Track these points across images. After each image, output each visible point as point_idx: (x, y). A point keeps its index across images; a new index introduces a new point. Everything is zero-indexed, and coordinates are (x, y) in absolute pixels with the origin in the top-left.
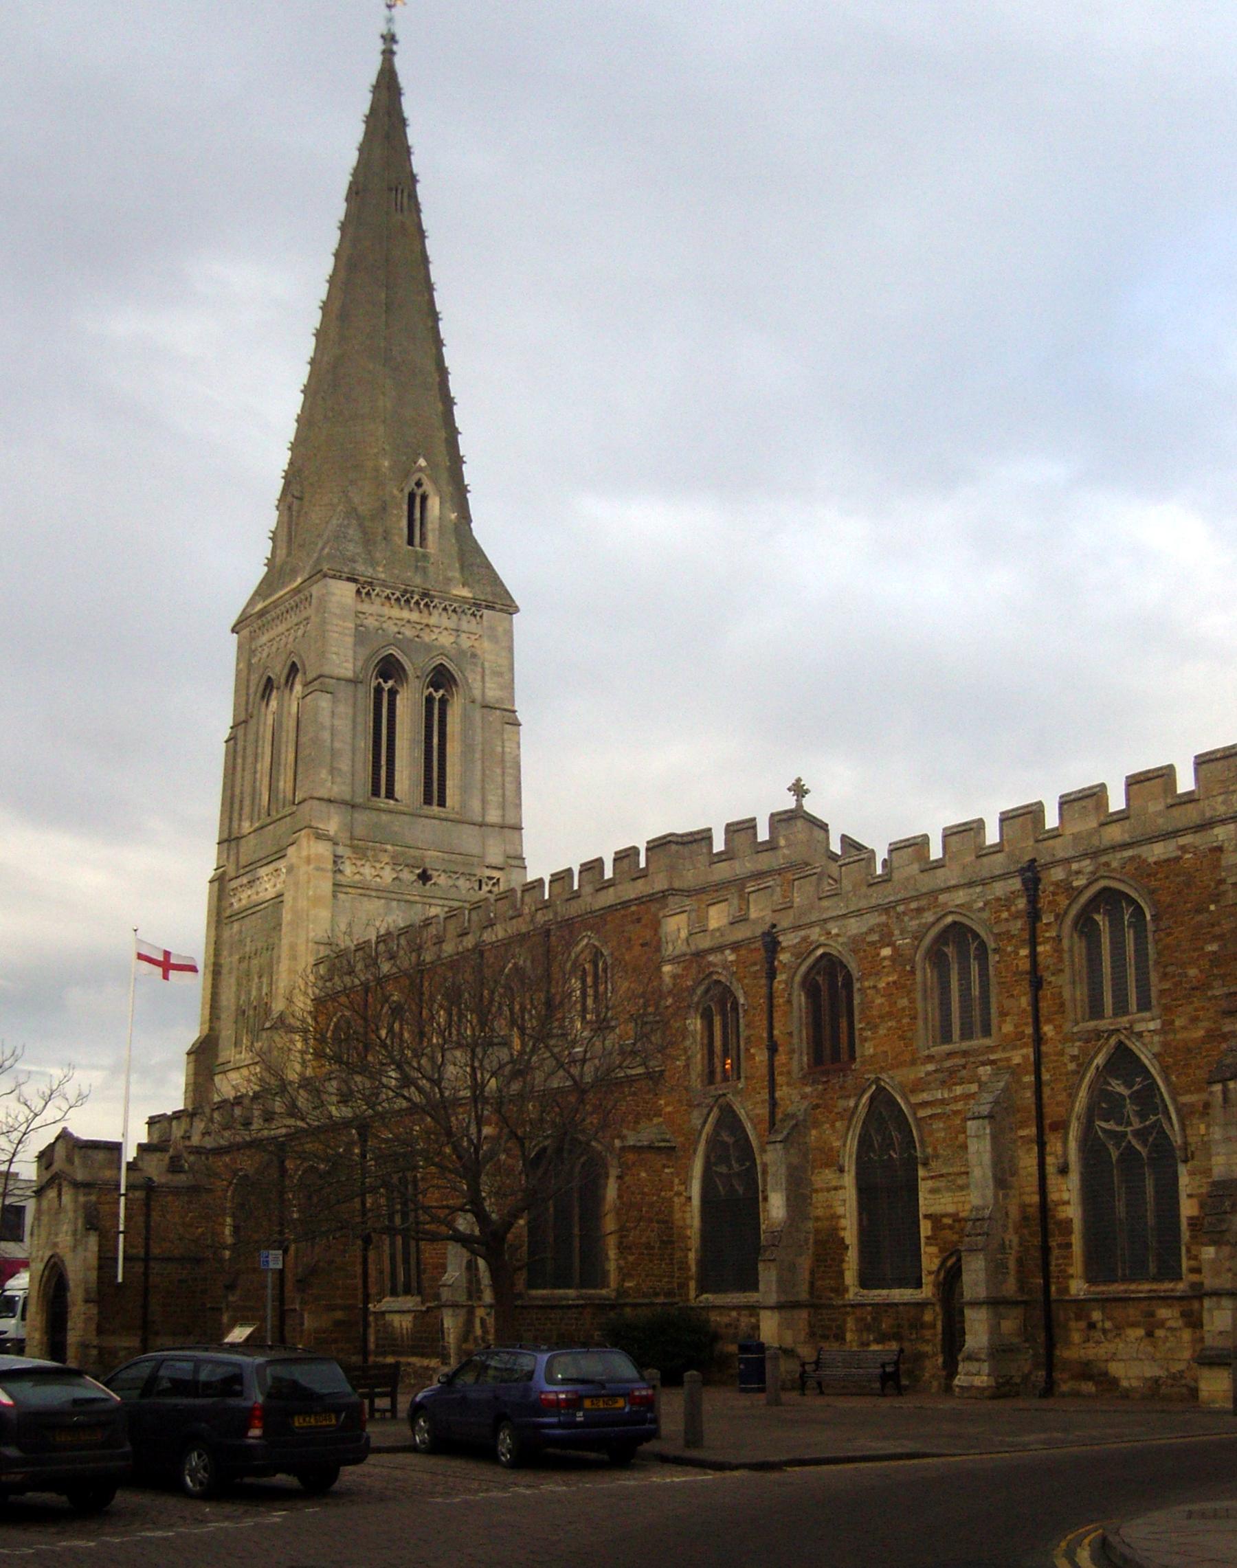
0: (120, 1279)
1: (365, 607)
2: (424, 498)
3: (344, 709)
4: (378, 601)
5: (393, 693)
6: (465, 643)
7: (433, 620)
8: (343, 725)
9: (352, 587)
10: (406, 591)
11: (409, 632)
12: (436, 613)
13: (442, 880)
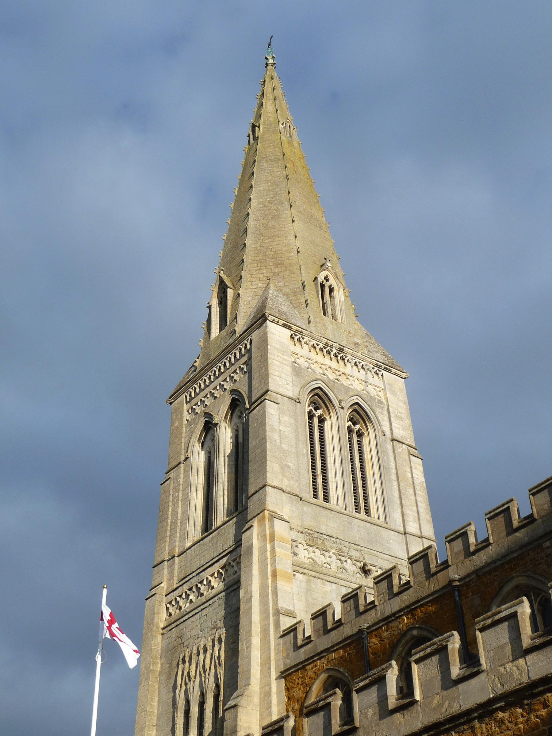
0: (105, 591)
1: (297, 349)
2: (331, 290)
4: (306, 347)
9: (288, 332)
10: (327, 344)
11: (332, 377)
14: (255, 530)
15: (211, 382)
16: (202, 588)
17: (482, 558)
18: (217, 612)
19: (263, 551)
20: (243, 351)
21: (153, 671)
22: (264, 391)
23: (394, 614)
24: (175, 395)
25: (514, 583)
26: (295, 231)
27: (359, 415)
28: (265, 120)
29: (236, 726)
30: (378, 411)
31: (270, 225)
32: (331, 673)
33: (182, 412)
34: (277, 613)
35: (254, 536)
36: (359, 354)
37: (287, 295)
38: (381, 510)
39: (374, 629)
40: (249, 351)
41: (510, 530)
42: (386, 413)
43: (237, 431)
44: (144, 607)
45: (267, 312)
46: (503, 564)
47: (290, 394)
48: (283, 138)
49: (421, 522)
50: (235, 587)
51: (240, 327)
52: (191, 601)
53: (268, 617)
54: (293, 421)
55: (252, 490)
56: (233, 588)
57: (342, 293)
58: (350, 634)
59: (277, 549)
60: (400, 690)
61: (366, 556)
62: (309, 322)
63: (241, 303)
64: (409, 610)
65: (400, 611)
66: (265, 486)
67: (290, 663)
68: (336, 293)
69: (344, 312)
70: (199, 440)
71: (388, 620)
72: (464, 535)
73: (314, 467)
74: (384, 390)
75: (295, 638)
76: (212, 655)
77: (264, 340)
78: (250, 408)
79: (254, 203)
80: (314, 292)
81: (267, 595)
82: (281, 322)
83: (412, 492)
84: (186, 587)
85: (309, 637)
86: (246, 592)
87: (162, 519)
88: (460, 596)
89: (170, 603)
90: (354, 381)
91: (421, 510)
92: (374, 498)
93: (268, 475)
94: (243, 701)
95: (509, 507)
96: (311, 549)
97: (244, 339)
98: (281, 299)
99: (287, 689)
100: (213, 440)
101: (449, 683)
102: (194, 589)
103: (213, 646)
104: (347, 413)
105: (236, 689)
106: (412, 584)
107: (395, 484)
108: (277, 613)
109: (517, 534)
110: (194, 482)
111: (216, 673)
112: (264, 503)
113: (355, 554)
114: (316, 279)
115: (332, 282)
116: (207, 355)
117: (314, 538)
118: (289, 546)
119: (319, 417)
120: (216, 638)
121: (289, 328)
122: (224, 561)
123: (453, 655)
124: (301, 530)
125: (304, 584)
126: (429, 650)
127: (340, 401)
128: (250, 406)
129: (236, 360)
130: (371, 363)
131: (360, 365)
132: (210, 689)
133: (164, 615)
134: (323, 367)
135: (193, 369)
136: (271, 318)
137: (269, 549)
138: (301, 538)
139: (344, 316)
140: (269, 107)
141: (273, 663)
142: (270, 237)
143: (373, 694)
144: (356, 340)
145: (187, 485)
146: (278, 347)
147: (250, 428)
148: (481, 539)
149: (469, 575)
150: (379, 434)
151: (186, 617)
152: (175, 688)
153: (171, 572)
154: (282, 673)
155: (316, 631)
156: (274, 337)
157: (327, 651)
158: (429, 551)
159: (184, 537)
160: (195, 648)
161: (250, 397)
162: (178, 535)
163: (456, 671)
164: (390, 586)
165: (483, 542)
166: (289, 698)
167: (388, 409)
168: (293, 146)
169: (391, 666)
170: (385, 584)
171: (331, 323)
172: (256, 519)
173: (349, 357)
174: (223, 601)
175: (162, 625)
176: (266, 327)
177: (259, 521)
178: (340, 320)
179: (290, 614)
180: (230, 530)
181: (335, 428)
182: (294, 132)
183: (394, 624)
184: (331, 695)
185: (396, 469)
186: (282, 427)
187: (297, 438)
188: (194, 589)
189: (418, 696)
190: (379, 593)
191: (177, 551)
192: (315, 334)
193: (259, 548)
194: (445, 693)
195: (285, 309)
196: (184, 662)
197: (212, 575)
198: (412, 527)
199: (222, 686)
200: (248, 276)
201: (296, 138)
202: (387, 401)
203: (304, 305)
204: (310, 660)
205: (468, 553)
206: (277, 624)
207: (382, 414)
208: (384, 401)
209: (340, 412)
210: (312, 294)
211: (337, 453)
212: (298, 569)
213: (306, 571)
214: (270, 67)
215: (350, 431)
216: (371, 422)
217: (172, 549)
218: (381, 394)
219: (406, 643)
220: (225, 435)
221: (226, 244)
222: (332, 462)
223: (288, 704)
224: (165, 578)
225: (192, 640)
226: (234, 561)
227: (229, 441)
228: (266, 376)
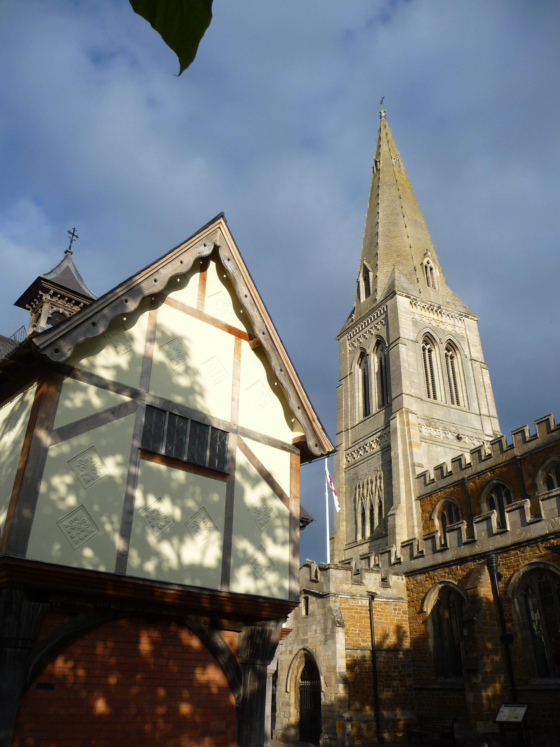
1: (414, 309)
2: (431, 269)
9: (408, 300)
10: (431, 305)
11: (435, 324)
13: (467, 440)
14: (398, 419)
15: (363, 329)
16: (367, 448)
17: (533, 445)
18: (377, 462)
19: (403, 431)
20: (382, 312)
21: (342, 492)
22: (397, 337)
23: (483, 471)
24: (341, 335)
25: (551, 459)
26: (408, 234)
27: (451, 346)
28: (383, 157)
29: (395, 525)
30: (462, 342)
31: (392, 229)
32: (447, 499)
33: (346, 346)
34: (414, 465)
35: (397, 422)
36: (450, 309)
37: (405, 275)
38: (466, 402)
39: (471, 478)
40: (386, 312)
41: (549, 431)
42: (466, 343)
43: (381, 358)
45: (396, 289)
46: (545, 449)
47: (412, 338)
48: (395, 168)
49: (490, 407)
50: (387, 449)
51: (379, 296)
52: (361, 455)
53: (408, 467)
54: (414, 354)
55: (394, 396)
56: (386, 450)
57: (438, 271)
58: (457, 480)
59: (411, 430)
60: (498, 524)
61: (459, 429)
62: (420, 292)
63: (379, 281)
64: (491, 469)
65: (486, 470)
66: (402, 394)
67: (422, 492)
68: (434, 271)
69: (440, 283)
70: (358, 362)
71: (479, 474)
72: (523, 432)
73: (427, 380)
74: (465, 329)
75: (425, 479)
76: (376, 485)
77: (395, 307)
78: (389, 346)
79: (381, 215)
80: (421, 272)
81: (407, 455)
82: (405, 294)
83: (484, 390)
84: (357, 447)
85: (433, 479)
86: (395, 453)
87: (339, 408)
88: (521, 464)
89: (348, 455)
90: (449, 325)
91: (489, 400)
92: (462, 395)
93: (403, 388)
94: (398, 512)
95: (548, 419)
96: (428, 428)
97: (382, 305)
98: (403, 279)
99: (422, 506)
100: (366, 362)
101: (524, 524)
102: (362, 448)
103: (376, 480)
104: (444, 345)
105: (392, 505)
106: (493, 456)
107: (473, 386)
108: (414, 465)
109: (553, 434)
110: (356, 387)
111: (379, 495)
112: (402, 404)
113: (453, 429)
114: (422, 264)
115: (432, 264)
117: (430, 422)
118: (417, 428)
119: (429, 349)
120: (378, 476)
122: (379, 434)
123: (527, 511)
124: (423, 417)
125: (426, 448)
126: (514, 507)
127: (440, 339)
128: (389, 346)
129: (378, 317)
130: (457, 313)
131: (450, 316)
132: (376, 503)
133: (345, 461)
134: (430, 319)
135: (350, 319)
136: (398, 293)
137: (406, 430)
138: (423, 422)
139: (440, 285)
140: (384, 148)
141: (412, 492)
142: (392, 238)
143: (484, 525)
144: (448, 300)
145: (353, 389)
146: (404, 310)
147: (390, 359)
148: (532, 434)
149: (526, 453)
150: (463, 357)
151: (358, 464)
152: (355, 501)
153: (347, 437)
154: (418, 497)
155: (436, 476)
156: (401, 304)
157: (444, 487)
158: (502, 439)
159: (353, 419)
160: (365, 481)
161: (388, 340)
162: (349, 417)
163: (529, 518)
164: (480, 456)
165: (533, 436)
166: (423, 511)
167: (468, 341)
168: (401, 173)
169: (493, 512)
170: (476, 454)
171: (433, 291)
172: (398, 413)
173: (444, 311)
174: (380, 456)
175: (344, 467)
176: (396, 298)
177: (400, 414)
178: (437, 289)
179: (421, 466)
180: (381, 418)
181: (438, 355)
182: (401, 164)
183: (482, 476)
184: (461, 523)
185: (474, 377)
186: (408, 358)
187: (418, 365)
188: (362, 448)
189: (509, 529)
190: (473, 459)
191: (350, 427)
192: (424, 300)
193: (401, 429)
194: (523, 528)
195: (405, 285)
196: (359, 488)
197: (373, 441)
198: (484, 411)
199: (383, 502)
200: (382, 264)
201: (403, 168)
202: (467, 336)
203: (416, 282)
205: (525, 442)
206: (414, 471)
207: (465, 344)
208: (465, 336)
209: (441, 345)
210: (420, 273)
211: (440, 370)
212: (422, 440)
214: (383, 118)
215: (446, 356)
216: (458, 350)
217: (346, 425)
218: (463, 332)
219: (490, 487)
220: (374, 361)
221: (365, 241)
222: (437, 376)
223: (422, 514)
224: (344, 441)
225: (363, 476)
226: (385, 434)
227: (376, 364)
228: (397, 329)
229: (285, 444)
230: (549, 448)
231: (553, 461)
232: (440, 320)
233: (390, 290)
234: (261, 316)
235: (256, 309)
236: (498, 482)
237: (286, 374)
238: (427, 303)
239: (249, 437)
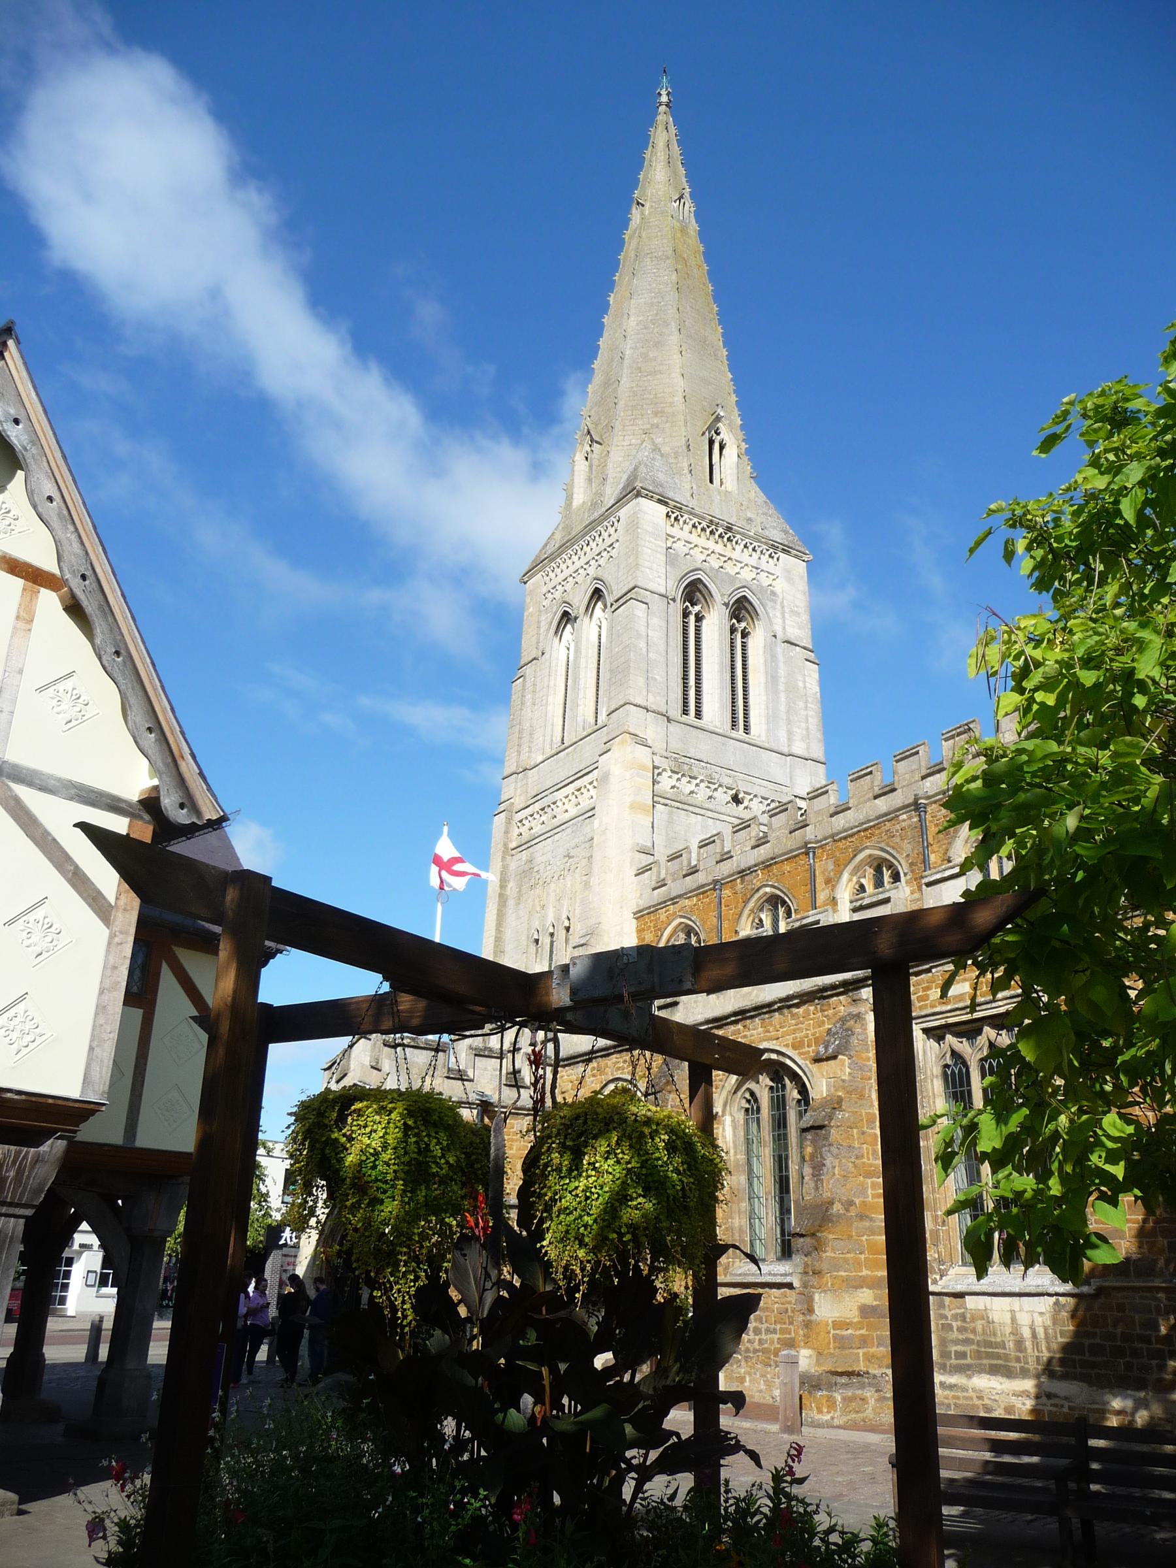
1: (675, 531)
2: (722, 447)
3: (655, 621)
5: (699, 618)
6: (764, 580)
7: (735, 555)
8: (657, 636)
9: (664, 510)
12: (739, 548)
25: (867, 852)
30: (770, 604)
31: (651, 355)
44: (492, 822)
61: (740, 783)
67: (643, 903)
73: (685, 677)
113: (726, 781)
116: (567, 528)
121: (666, 504)
124: (665, 754)
125: (665, 817)
142: (650, 374)
144: (749, 515)
146: (650, 530)
168: (687, 234)
183: (747, 878)
192: (698, 510)
200: (621, 427)
204: (663, 904)
213: (668, 802)
219: (760, 898)
229: (119, 800)
230: (866, 830)
231: (870, 856)
232: (729, 555)
233: (628, 485)
234: (82, 543)
235: (71, 528)
236: (774, 890)
237: (128, 663)
238: (703, 518)
239: (30, 784)
